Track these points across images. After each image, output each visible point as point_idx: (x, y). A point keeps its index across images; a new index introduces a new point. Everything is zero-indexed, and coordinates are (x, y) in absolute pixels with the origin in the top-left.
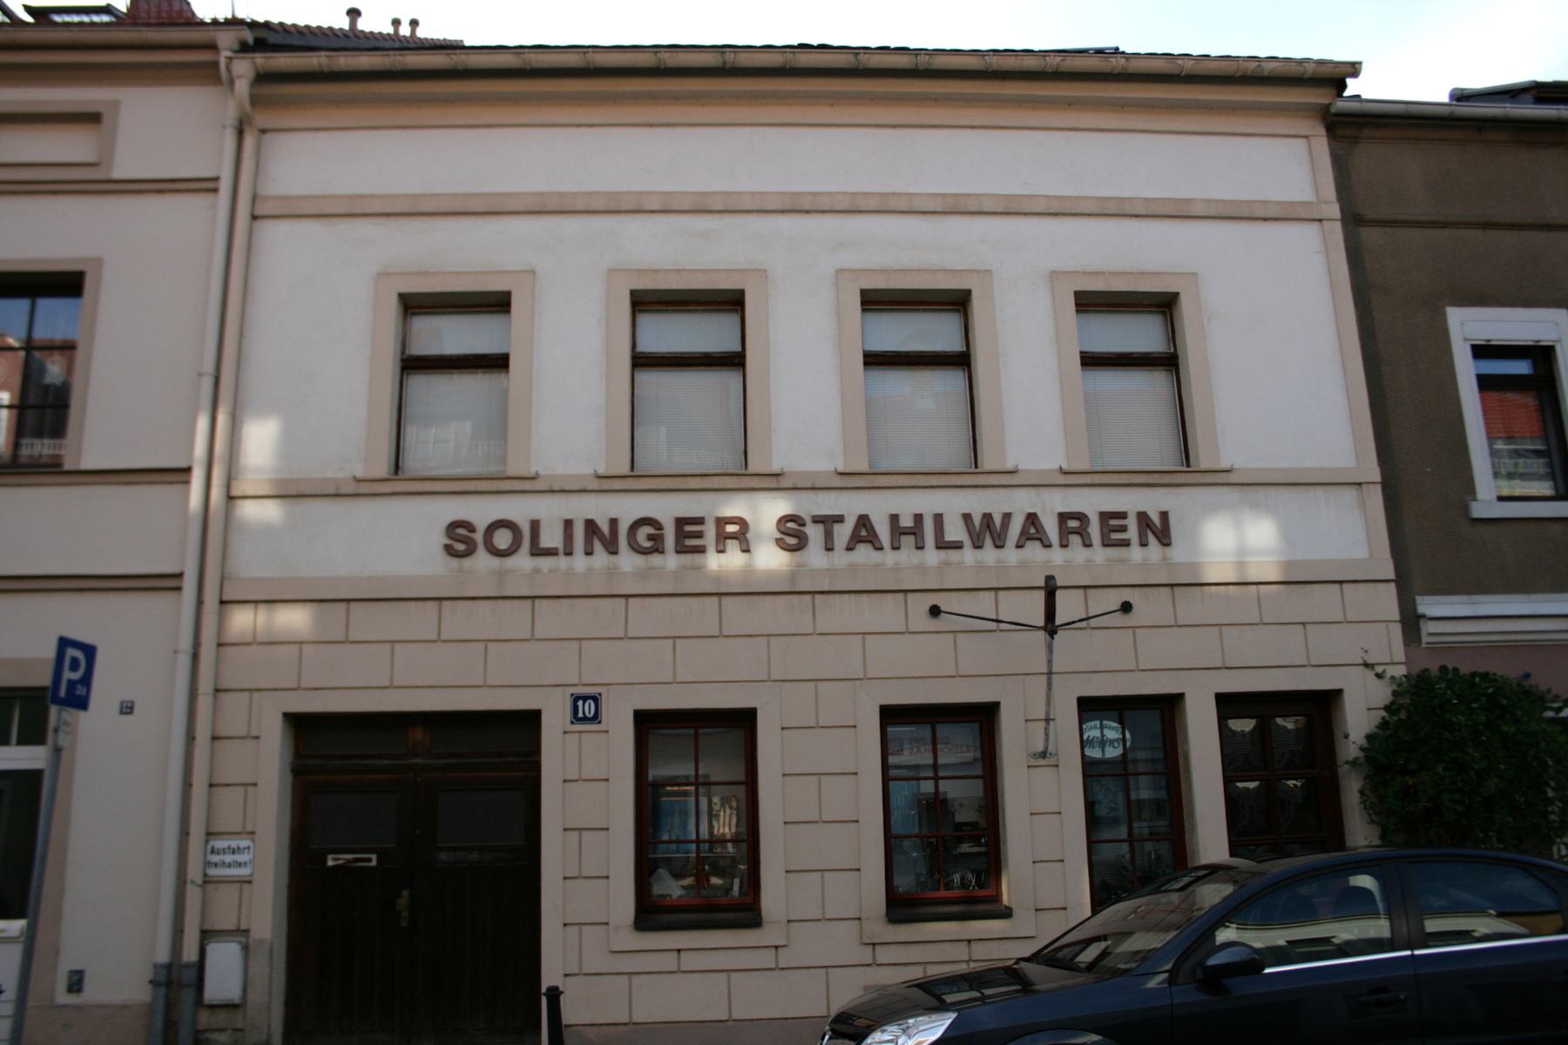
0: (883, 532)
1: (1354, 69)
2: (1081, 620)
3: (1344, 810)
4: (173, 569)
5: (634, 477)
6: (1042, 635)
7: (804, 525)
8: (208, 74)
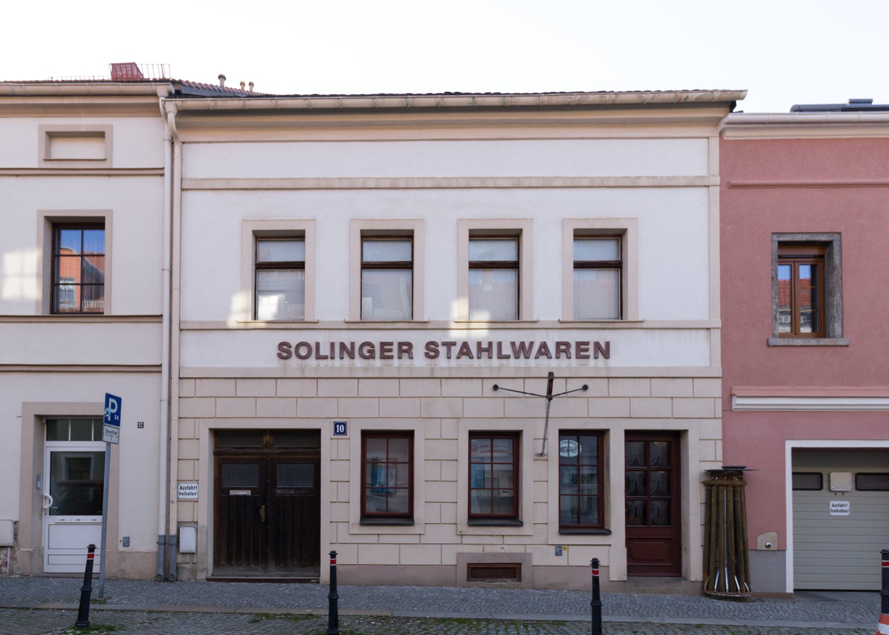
0: (474, 350)
1: (740, 95)
2: (563, 393)
3: (682, 487)
4: (159, 363)
5: (361, 324)
6: (545, 400)
7: (438, 346)
8: (154, 110)
